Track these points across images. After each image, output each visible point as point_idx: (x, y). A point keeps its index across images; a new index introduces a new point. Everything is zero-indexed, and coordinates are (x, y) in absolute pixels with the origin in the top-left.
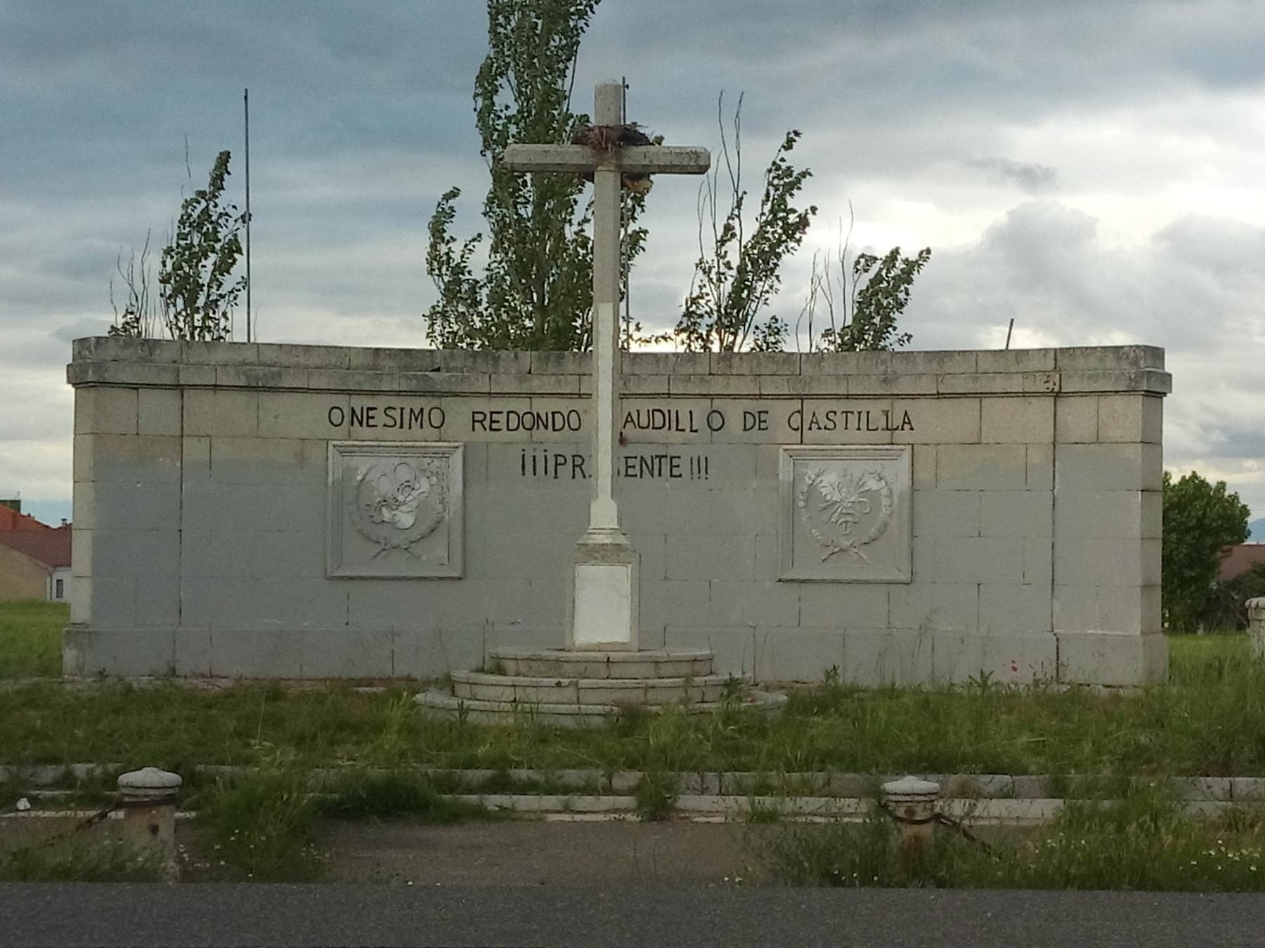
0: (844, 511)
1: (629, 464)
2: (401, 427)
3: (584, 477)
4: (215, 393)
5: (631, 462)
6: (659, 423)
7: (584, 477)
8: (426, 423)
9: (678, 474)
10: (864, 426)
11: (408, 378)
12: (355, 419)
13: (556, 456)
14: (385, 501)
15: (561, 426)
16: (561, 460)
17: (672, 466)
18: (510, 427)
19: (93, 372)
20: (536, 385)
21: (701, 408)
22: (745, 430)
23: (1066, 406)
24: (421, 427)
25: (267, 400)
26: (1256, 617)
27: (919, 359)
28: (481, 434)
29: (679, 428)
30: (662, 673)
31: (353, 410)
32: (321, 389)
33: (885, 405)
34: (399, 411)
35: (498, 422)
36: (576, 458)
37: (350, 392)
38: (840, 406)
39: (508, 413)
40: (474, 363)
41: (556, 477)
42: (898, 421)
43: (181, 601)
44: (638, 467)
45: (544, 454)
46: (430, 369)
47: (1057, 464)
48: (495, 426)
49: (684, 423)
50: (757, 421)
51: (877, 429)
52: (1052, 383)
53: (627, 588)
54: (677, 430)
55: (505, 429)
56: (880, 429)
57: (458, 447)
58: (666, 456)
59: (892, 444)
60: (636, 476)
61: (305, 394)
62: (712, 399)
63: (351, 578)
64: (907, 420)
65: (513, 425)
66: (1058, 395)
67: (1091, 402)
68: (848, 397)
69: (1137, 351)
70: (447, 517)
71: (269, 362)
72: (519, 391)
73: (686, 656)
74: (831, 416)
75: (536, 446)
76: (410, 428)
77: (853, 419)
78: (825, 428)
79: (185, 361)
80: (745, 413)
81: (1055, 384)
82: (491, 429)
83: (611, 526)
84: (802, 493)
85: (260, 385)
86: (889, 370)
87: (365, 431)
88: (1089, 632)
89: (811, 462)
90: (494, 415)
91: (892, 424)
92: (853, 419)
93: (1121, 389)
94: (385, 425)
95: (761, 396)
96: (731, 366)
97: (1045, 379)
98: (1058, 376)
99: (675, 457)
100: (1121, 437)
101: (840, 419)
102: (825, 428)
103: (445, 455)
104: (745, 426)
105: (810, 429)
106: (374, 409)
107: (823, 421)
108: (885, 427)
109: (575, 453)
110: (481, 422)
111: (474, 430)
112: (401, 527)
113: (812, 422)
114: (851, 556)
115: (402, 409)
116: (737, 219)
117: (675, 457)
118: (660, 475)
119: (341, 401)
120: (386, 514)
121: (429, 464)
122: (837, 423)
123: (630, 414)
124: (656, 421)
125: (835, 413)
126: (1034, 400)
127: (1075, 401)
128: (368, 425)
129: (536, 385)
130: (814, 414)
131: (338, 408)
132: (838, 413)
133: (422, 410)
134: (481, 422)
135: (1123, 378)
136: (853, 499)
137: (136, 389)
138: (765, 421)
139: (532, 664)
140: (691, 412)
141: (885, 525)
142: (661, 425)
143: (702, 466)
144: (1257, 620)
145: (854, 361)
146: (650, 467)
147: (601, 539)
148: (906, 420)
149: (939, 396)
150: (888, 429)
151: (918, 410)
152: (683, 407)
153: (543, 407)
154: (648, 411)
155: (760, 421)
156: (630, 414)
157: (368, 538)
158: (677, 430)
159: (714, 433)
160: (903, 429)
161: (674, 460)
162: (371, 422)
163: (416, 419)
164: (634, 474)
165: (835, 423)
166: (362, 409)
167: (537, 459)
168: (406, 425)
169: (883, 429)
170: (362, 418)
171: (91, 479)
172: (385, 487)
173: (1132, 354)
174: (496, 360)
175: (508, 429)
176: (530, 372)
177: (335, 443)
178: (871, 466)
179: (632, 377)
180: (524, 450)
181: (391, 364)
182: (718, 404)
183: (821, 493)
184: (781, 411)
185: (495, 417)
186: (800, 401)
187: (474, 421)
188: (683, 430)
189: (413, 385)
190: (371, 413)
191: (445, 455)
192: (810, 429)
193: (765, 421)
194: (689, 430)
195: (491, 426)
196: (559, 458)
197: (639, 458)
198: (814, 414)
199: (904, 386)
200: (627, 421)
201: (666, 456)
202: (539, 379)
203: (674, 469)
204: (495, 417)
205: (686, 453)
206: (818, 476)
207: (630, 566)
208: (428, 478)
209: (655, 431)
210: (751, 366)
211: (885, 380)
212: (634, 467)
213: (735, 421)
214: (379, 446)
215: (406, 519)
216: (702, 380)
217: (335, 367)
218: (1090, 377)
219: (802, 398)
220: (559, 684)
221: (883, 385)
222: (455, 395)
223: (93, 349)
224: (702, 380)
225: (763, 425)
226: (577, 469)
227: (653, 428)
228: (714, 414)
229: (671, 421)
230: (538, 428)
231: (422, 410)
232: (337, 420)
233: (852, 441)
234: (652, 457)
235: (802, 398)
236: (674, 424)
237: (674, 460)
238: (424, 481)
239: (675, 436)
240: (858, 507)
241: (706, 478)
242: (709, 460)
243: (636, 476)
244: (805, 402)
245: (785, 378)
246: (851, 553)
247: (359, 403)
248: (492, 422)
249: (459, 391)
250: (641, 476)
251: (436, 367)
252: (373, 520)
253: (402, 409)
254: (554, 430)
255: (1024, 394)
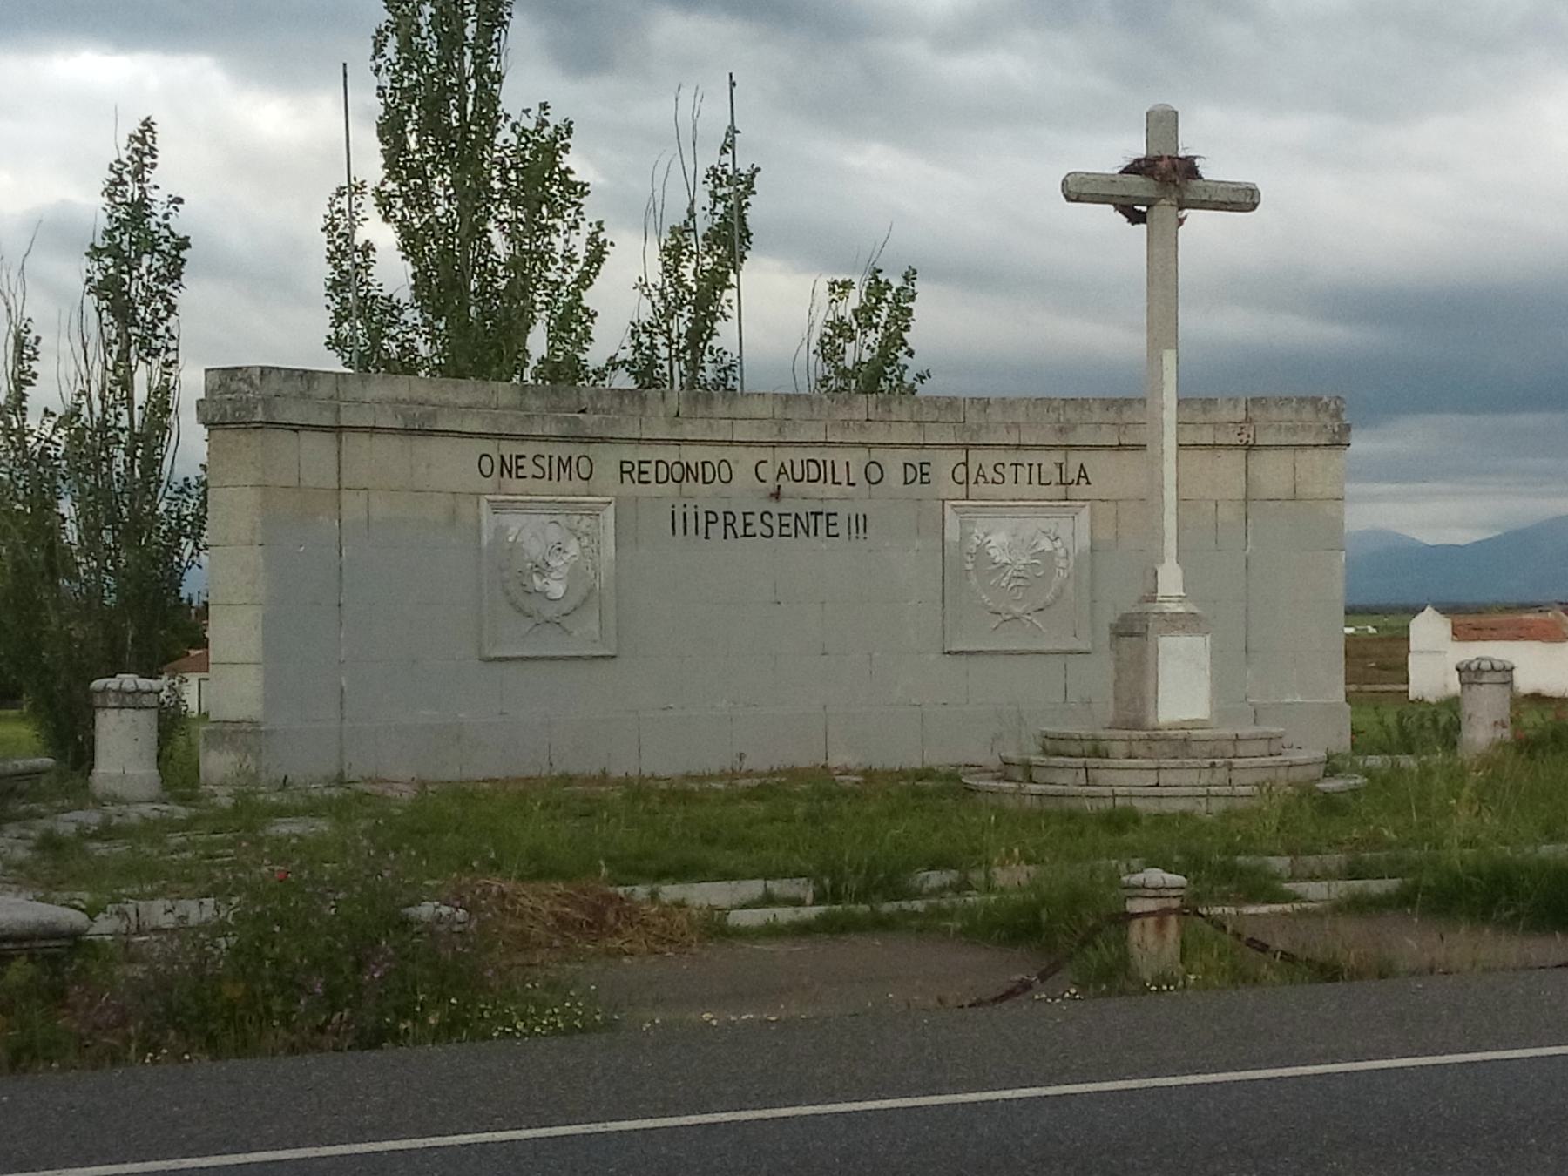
0: (1015, 574)
1: (783, 522)
2: (550, 479)
3: (736, 537)
4: (371, 436)
5: (785, 520)
6: (813, 476)
7: (736, 537)
8: (574, 475)
9: (835, 533)
10: (1035, 479)
11: (559, 421)
12: (504, 469)
13: (707, 513)
14: (537, 566)
15: (711, 478)
16: (712, 517)
17: (828, 525)
18: (660, 480)
19: (263, 409)
20: (689, 430)
21: (858, 457)
22: (906, 483)
23: (1257, 458)
24: (570, 479)
25: (419, 444)
26: (1476, 680)
27: (1096, 407)
28: (631, 488)
29: (836, 481)
30: (1241, 752)
31: (502, 457)
32: (474, 433)
33: (1058, 456)
34: (547, 458)
35: (646, 473)
36: (727, 516)
37: (499, 436)
38: (1009, 457)
39: (657, 462)
40: (621, 403)
41: (707, 538)
42: (1074, 475)
43: (342, 691)
44: (792, 526)
45: (694, 510)
46: (577, 410)
47: (1249, 521)
48: (644, 477)
49: (841, 476)
50: (919, 474)
51: (1050, 484)
52: (1246, 436)
53: (1205, 660)
54: (834, 483)
55: (654, 481)
56: (1053, 483)
57: (610, 503)
58: (821, 513)
59: (1067, 500)
60: (789, 536)
61: (456, 439)
62: (341, 432)
63: (507, 659)
64: (1083, 473)
65: (662, 476)
66: (1249, 448)
67: (1286, 455)
68: (1018, 447)
69: (1338, 402)
70: (598, 586)
71: (420, 400)
72: (669, 437)
73: (1264, 733)
74: (999, 468)
75: (686, 501)
76: (559, 479)
77: (1023, 473)
78: (993, 482)
79: (342, 397)
80: (905, 464)
81: (1249, 436)
82: (640, 482)
83: (1178, 594)
84: (971, 555)
85: (417, 427)
86: (1062, 419)
87: (516, 484)
88: (1287, 700)
89: (978, 520)
90: (643, 465)
91: (1066, 477)
92: (1023, 473)
93: (1323, 443)
94: (534, 476)
95: (923, 446)
96: (890, 411)
97: (1239, 431)
98: (1252, 428)
99: (831, 514)
100: (1321, 494)
101: (1009, 472)
102: (993, 482)
103: (594, 512)
104: (906, 479)
105: (976, 482)
106: (523, 457)
107: (990, 474)
108: (1059, 481)
109: (726, 510)
110: (629, 473)
111: (622, 482)
112: (554, 597)
113: (978, 475)
114: (1024, 624)
115: (550, 457)
116: (692, 234)
117: (831, 514)
118: (816, 534)
119: (489, 446)
120: (538, 582)
121: (578, 523)
122: (1006, 476)
123: (782, 465)
124: (811, 473)
125: (1003, 465)
126: (1222, 453)
127: (1270, 455)
128: (518, 477)
129: (689, 430)
130: (981, 466)
131: (585, 456)
132: (1007, 465)
133: (570, 458)
134: (629, 473)
135: (1324, 430)
136: (1024, 561)
137: (296, 431)
138: (927, 474)
139: (1152, 744)
140: (847, 463)
141: (1062, 589)
142: (816, 478)
143: (861, 524)
144: (1476, 683)
145: (1023, 409)
146: (799, 524)
147: (1173, 607)
148: (1082, 474)
149: (1121, 447)
150: (1062, 484)
151: (1094, 462)
152: (839, 456)
153: (693, 455)
154: (802, 462)
155: (922, 474)
156: (782, 465)
157: (520, 610)
158: (834, 483)
159: (873, 487)
160: (1078, 483)
161: (830, 517)
162: (521, 472)
163: (565, 471)
164: (788, 533)
165: (1003, 477)
166: (511, 456)
167: (688, 516)
168: (555, 477)
169: (1057, 484)
170: (511, 468)
171: (259, 538)
172: (535, 549)
173: (1332, 406)
174: (643, 400)
175: (657, 482)
176: (678, 415)
177: (491, 497)
178: (1043, 524)
179: (787, 423)
180: (696, 507)
181: (538, 403)
182: (877, 454)
183: (989, 554)
184: (945, 462)
185: (644, 467)
186: (965, 452)
187: (622, 472)
188: (840, 484)
189: (564, 429)
190: (521, 462)
191: (594, 512)
192: (976, 482)
193: (927, 474)
194: (845, 482)
195: (639, 478)
196: (710, 515)
197: (793, 516)
198: (981, 466)
199: (1082, 436)
200: (780, 473)
201: (821, 513)
202: (691, 423)
203: (783, 528)
204: (644, 467)
205: (844, 510)
206: (986, 535)
207: (1208, 637)
208: (579, 539)
209: (809, 484)
210: (912, 411)
211: (1061, 430)
212: (788, 525)
213: (895, 474)
214: (531, 501)
215: (557, 589)
216: (861, 426)
217: (486, 406)
218: (1288, 429)
219: (967, 448)
220: (1213, 765)
221: (1059, 435)
222: (602, 440)
223: (257, 382)
224: (861, 426)
225: (925, 479)
226: (729, 528)
227: (808, 481)
228: (872, 465)
229: (826, 473)
230: (688, 480)
231: (570, 458)
232: (487, 470)
233: (1025, 497)
234: (807, 514)
235: (967, 448)
236: (829, 476)
237: (830, 517)
238: (574, 541)
239: (831, 491)
240: (1030, 570)
241: (865, 538)
242: (868, 517)
243: (789, 536)
244: (970, 452)
245: (951, 425)
246: (1024, 621)
247: (509, 449)
248: (641, 473)
249: (610, 436)
250: (796, 536)
251: (583, 407)
252: (525, 589)
253: (550, 457)
254: (704, 483)
255: (1215, 447)
